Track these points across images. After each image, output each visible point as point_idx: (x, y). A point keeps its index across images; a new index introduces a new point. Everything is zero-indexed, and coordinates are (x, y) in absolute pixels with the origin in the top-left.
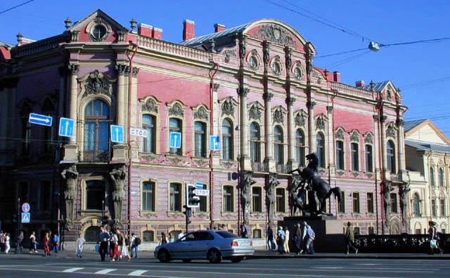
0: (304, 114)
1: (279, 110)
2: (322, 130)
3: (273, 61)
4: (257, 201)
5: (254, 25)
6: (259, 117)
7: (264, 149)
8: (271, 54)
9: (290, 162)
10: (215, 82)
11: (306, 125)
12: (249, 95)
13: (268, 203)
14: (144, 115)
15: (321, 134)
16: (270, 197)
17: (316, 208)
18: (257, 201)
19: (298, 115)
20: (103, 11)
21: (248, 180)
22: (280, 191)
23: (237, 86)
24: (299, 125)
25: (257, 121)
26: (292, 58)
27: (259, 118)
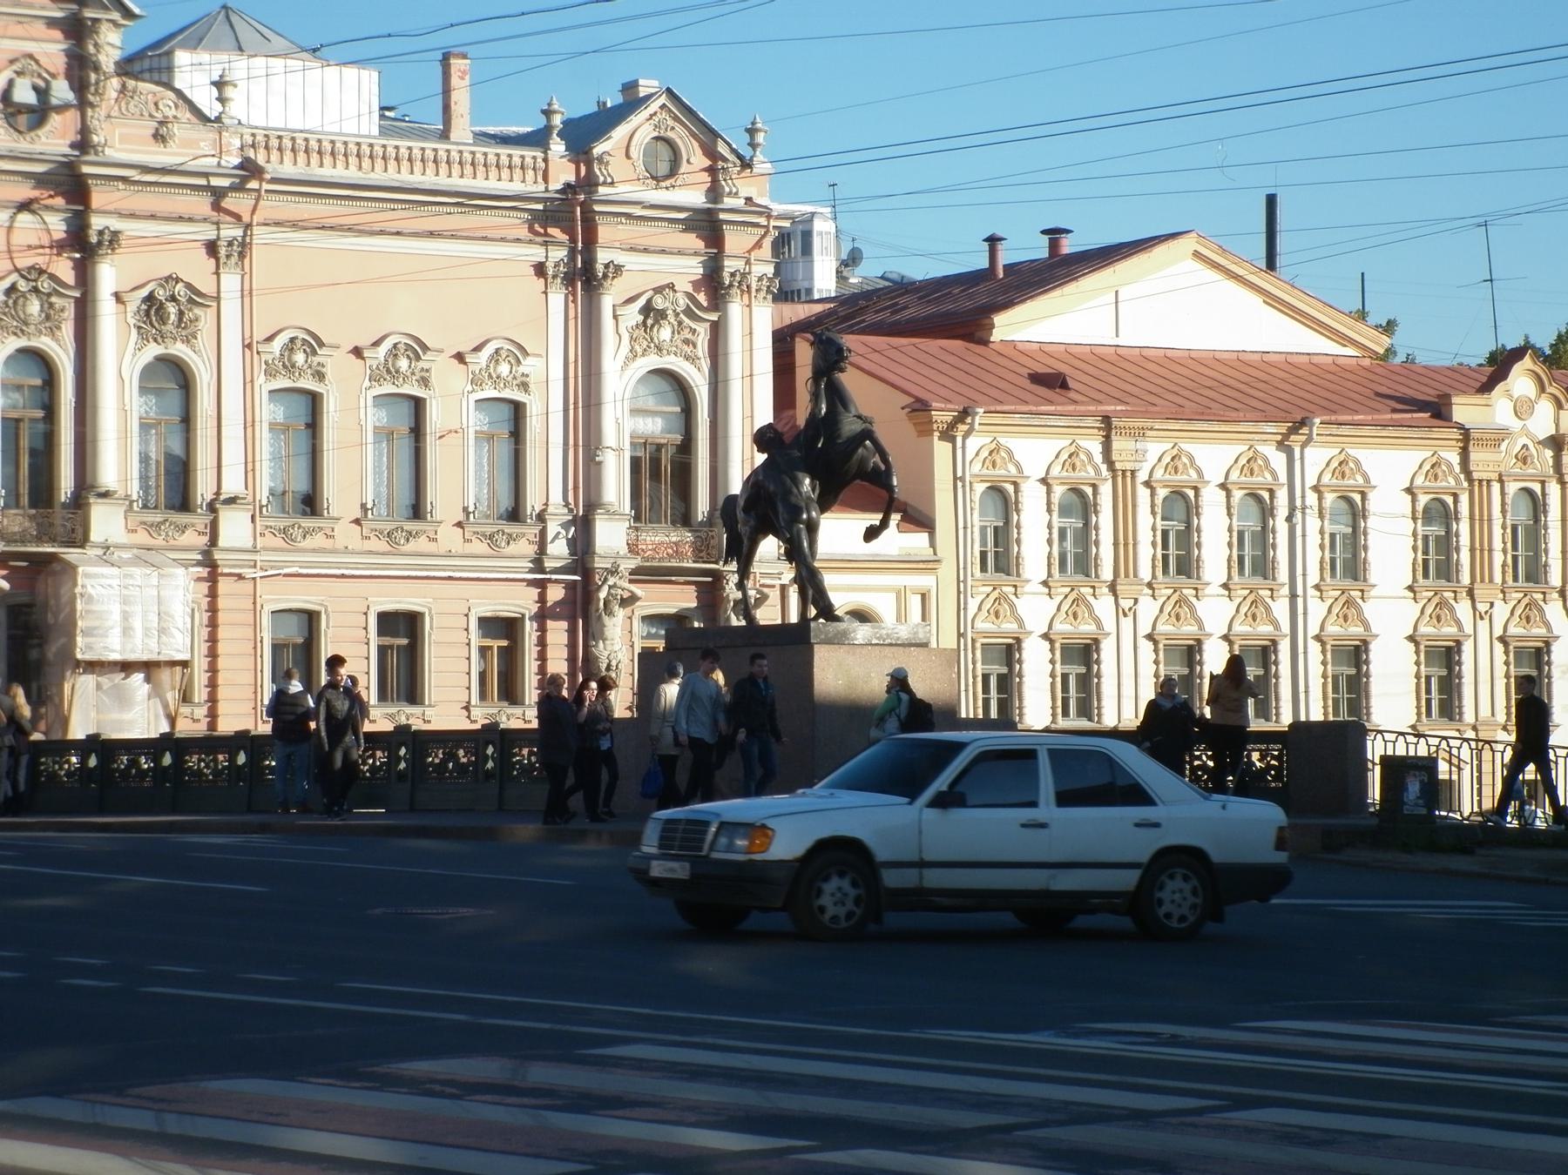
11: (68, 330)
24: (160, 338)
25: (44, 343)
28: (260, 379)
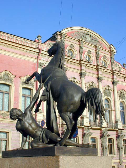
0: (110, 89)
1: (122, 92)
2: (124, 100)
3: (86, 54)
4: (111, 147)
5: (73, 29)
6: (111, 95)
7: (8, 99)
8: (101, 54)
9: (116, 122)
10: (39, 61)
11: (112, 96)
12: (103, 81)
13: (119, 149)
14: (23, 88)
16: (119, 145)
17: (51, 147)
18: (111, 147)
19: (106, 89)
20: (54, 33)
21: (105, 134)
22: (110, 140)
23: (112, 80)
26: (84, 48)
27: (110, 95)
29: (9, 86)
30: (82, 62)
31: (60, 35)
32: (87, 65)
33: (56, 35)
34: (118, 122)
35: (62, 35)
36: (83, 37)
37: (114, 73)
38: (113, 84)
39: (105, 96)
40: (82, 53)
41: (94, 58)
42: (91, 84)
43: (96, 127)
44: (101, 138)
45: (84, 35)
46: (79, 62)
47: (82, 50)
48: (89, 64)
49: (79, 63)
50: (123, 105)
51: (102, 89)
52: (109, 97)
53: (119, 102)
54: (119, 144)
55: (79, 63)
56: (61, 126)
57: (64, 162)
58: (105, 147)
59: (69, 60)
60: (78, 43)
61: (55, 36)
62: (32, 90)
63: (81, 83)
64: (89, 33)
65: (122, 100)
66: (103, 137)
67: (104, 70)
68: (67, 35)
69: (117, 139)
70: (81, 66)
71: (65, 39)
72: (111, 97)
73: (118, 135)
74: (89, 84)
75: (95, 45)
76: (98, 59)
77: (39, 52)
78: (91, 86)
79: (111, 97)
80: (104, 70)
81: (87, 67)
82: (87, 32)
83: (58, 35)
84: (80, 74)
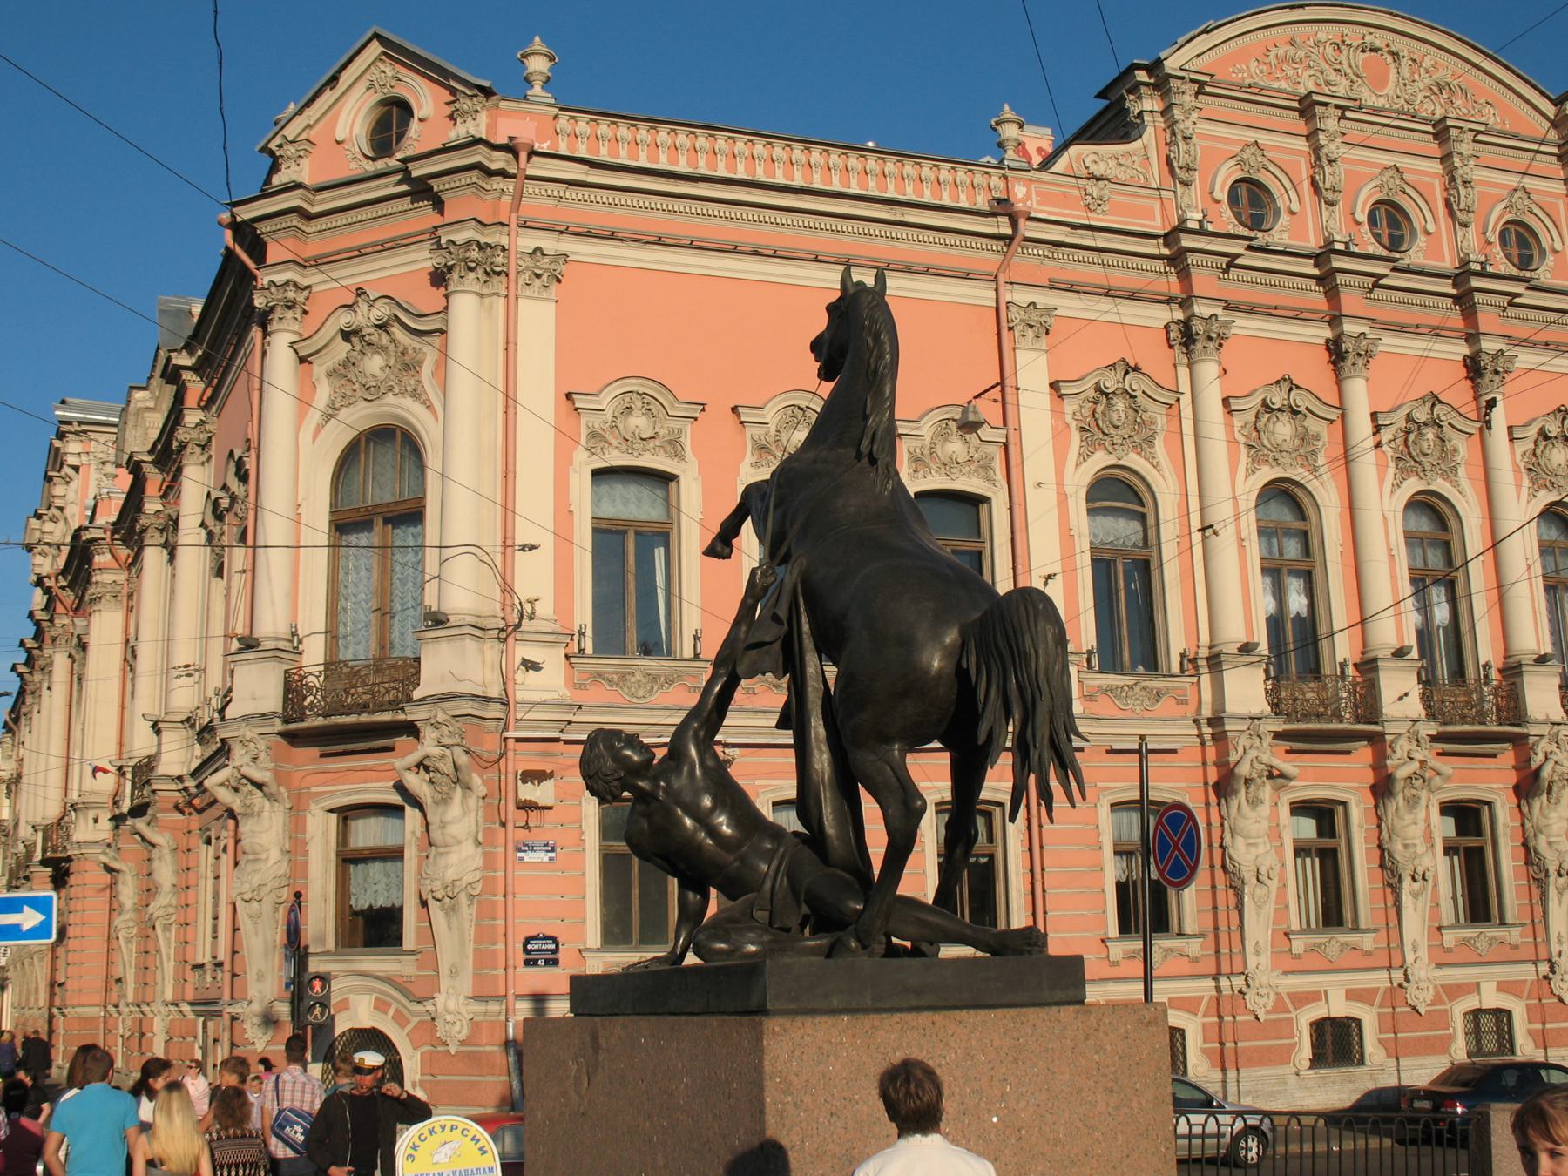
0: (1301, 400)
15: (1429, 507)
27: (1450, 473)
28: (580, 455)
29: (665, 479)
30: (1336, 264)
31: (1156, 87)
32: (1516, 300)
33: (1130, 92)
34: (1520, 674)
35: (1174, 83)
36: (1333, 76)
37: (1340, 277)
38: (1334, 363)
39: (1542, 493)
40: (1330, 196)
41: (1436, 222)
42: (1422, 415)
43: (1340, 726)
44: (1523, 802)
45: (1343, 58)
46: (1161, 241)
47: (1188, 153)
48: (1393, 270)
49: (1316, 272)
50: (1143, 505)
51: (1512, 440)
52: (1440, 485)
53: (1080, 479)
54: (1239, 841)
55: (1316, 272)
56: (1208, 738)
57: (797, 1053)
58: (1552, 869)
59: (1238, 261)
60: (1433, 148)
61: (1123, 99)
62: (986, 500)
63: (1343, 416)
64: (1379, 39)
65: (1112, 461)
66: (1235, 792)
67: (1519, 295)
68: (1207, 79)
69: (1523, 802)
70: (1188, 275)
71: (1195, 115)
72: (1456, 485)
73: (1527, 772)
74: (1409, 418)
75: (1438, 116)
76: (1331, 204)
77: (1009, 231)
78: (1421, 426)
79: (1456, 485)
80: (1519, 295)
81: (1511, 311)
82: (1364, 30)
83: (1143, 90)
84: (1328, 349)
